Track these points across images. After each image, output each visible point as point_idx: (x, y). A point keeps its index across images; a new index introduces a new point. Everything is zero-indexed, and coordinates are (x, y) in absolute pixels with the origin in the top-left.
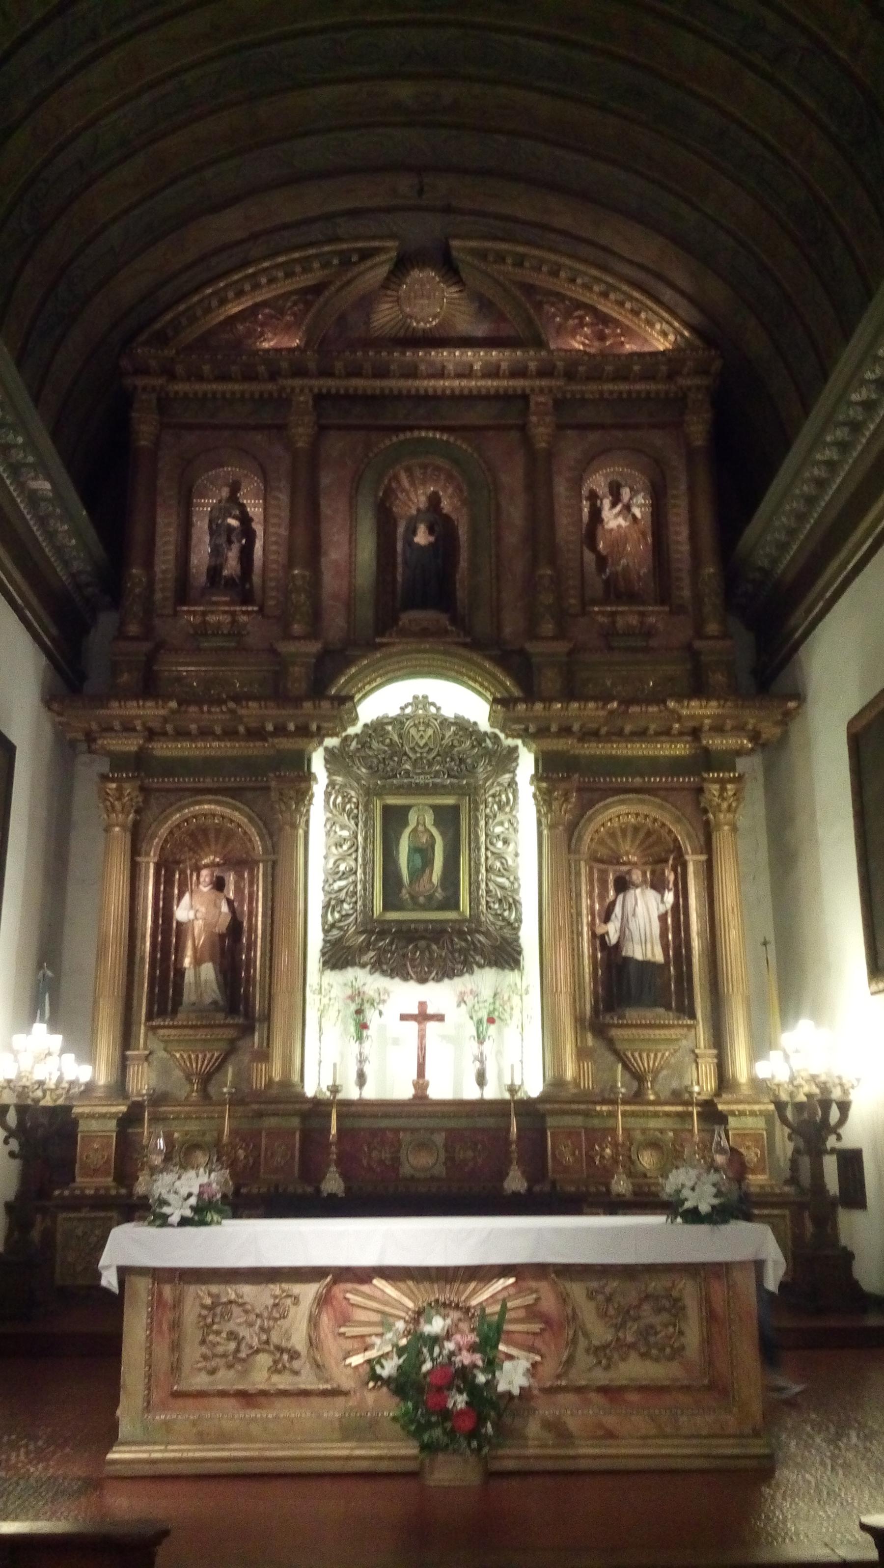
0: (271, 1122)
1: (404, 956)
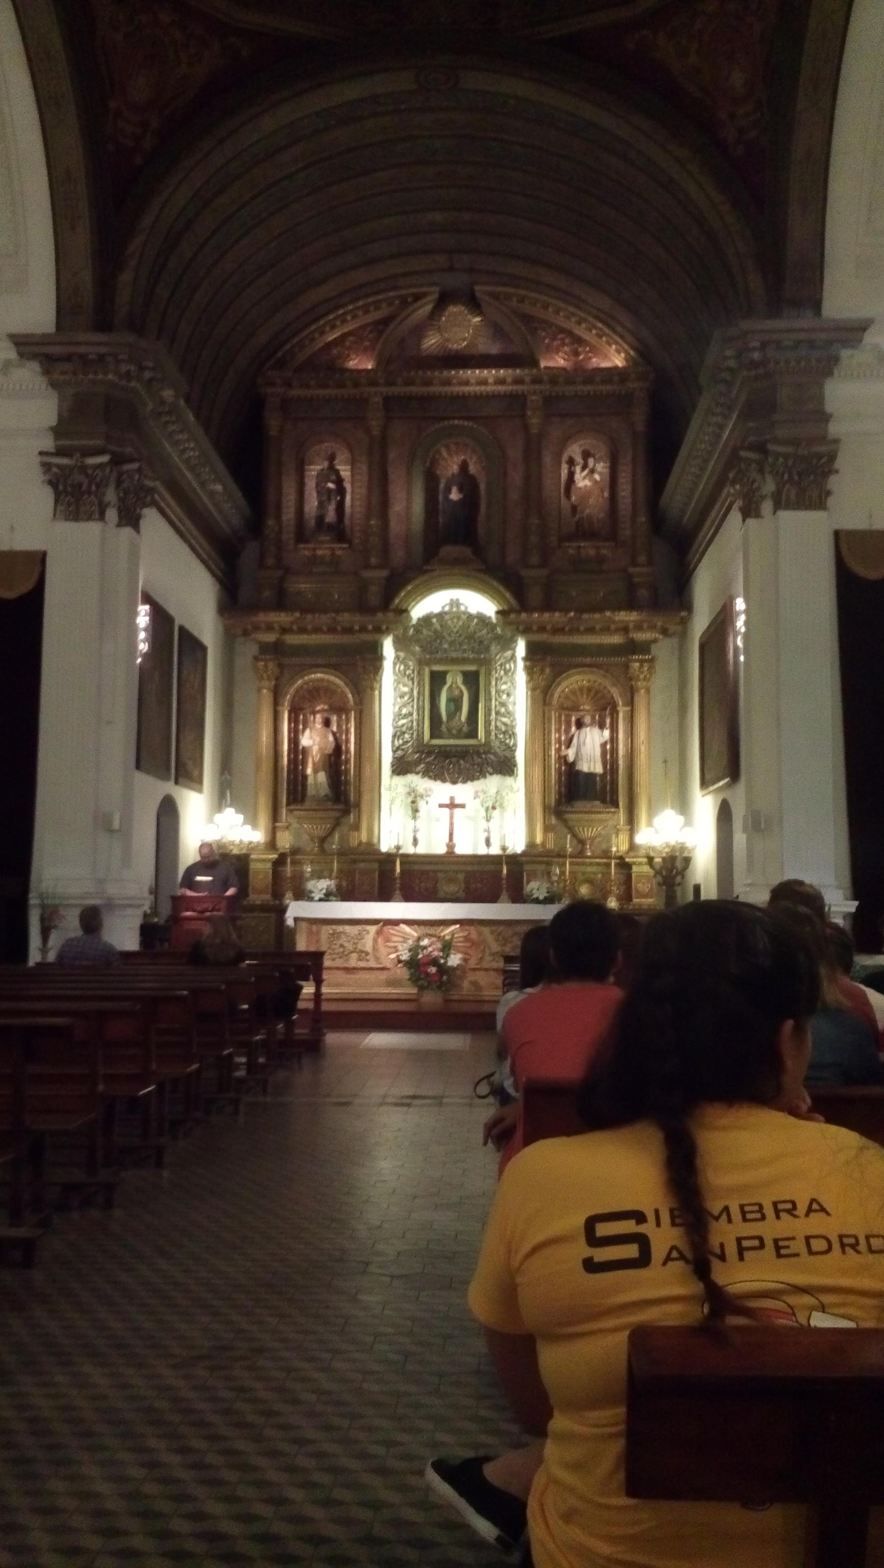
0: (362, 865)
1: (443, 767)
